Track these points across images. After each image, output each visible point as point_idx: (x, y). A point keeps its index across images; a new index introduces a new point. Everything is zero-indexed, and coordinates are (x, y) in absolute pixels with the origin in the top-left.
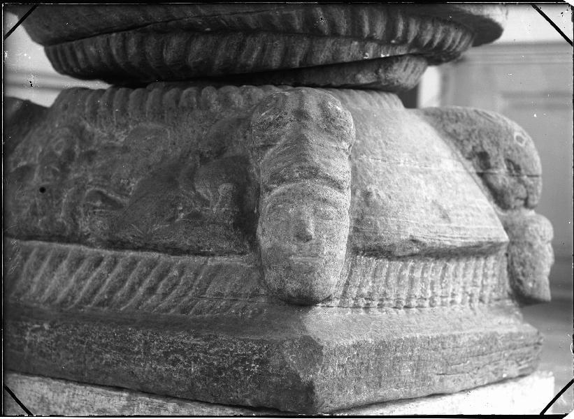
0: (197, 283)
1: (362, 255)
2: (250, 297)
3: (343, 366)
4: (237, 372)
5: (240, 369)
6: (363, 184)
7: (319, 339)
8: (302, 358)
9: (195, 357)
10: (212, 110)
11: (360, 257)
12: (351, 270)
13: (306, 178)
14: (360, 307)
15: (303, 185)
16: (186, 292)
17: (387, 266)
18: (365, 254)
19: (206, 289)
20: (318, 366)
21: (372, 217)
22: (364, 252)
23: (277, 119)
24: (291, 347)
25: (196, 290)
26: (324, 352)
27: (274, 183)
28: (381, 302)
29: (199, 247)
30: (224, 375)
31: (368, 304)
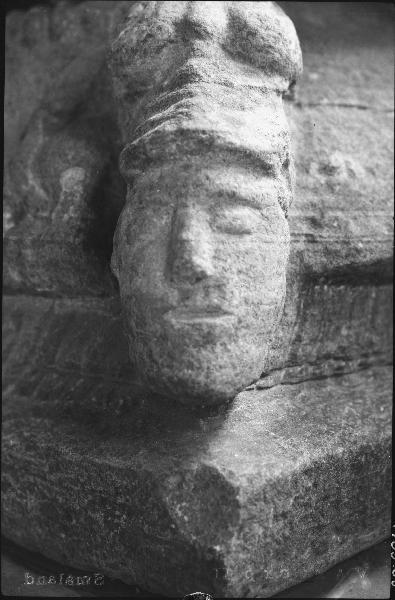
0: (40, 344)
1: (324, 283)
2: (120, 376)
3: (284, 515)
4: (93, 521)
5: (99, 516)
6: (322, 152)
7: (231, 473)
8: (202, 510)
9: (31, 484)
10: (63, 40)
11: (322, 288)
12: (304, 313)
13: (191, 153)
14: (325, 377)
15: (187, 167)
16: (26, 358)
17: (374, 295)
18: (330, 282)
19: (54, 356)
20: (231, 529)
21: (339, 214)
22: (327, 278)
23: (145, 41)
24: (179, 486)
25: (41, 356)
26: (241, 498)
27: (135, 167)
28: (364, 360)
29: (34, 285)
30: (74, 521)
31: (340, 368)
